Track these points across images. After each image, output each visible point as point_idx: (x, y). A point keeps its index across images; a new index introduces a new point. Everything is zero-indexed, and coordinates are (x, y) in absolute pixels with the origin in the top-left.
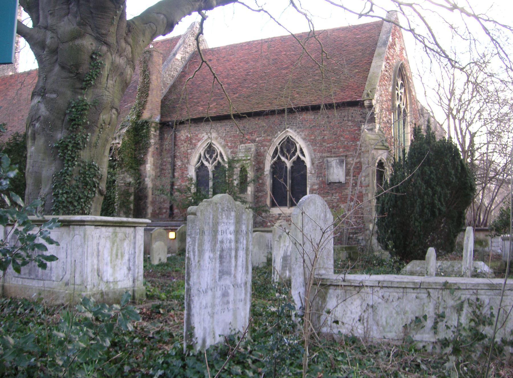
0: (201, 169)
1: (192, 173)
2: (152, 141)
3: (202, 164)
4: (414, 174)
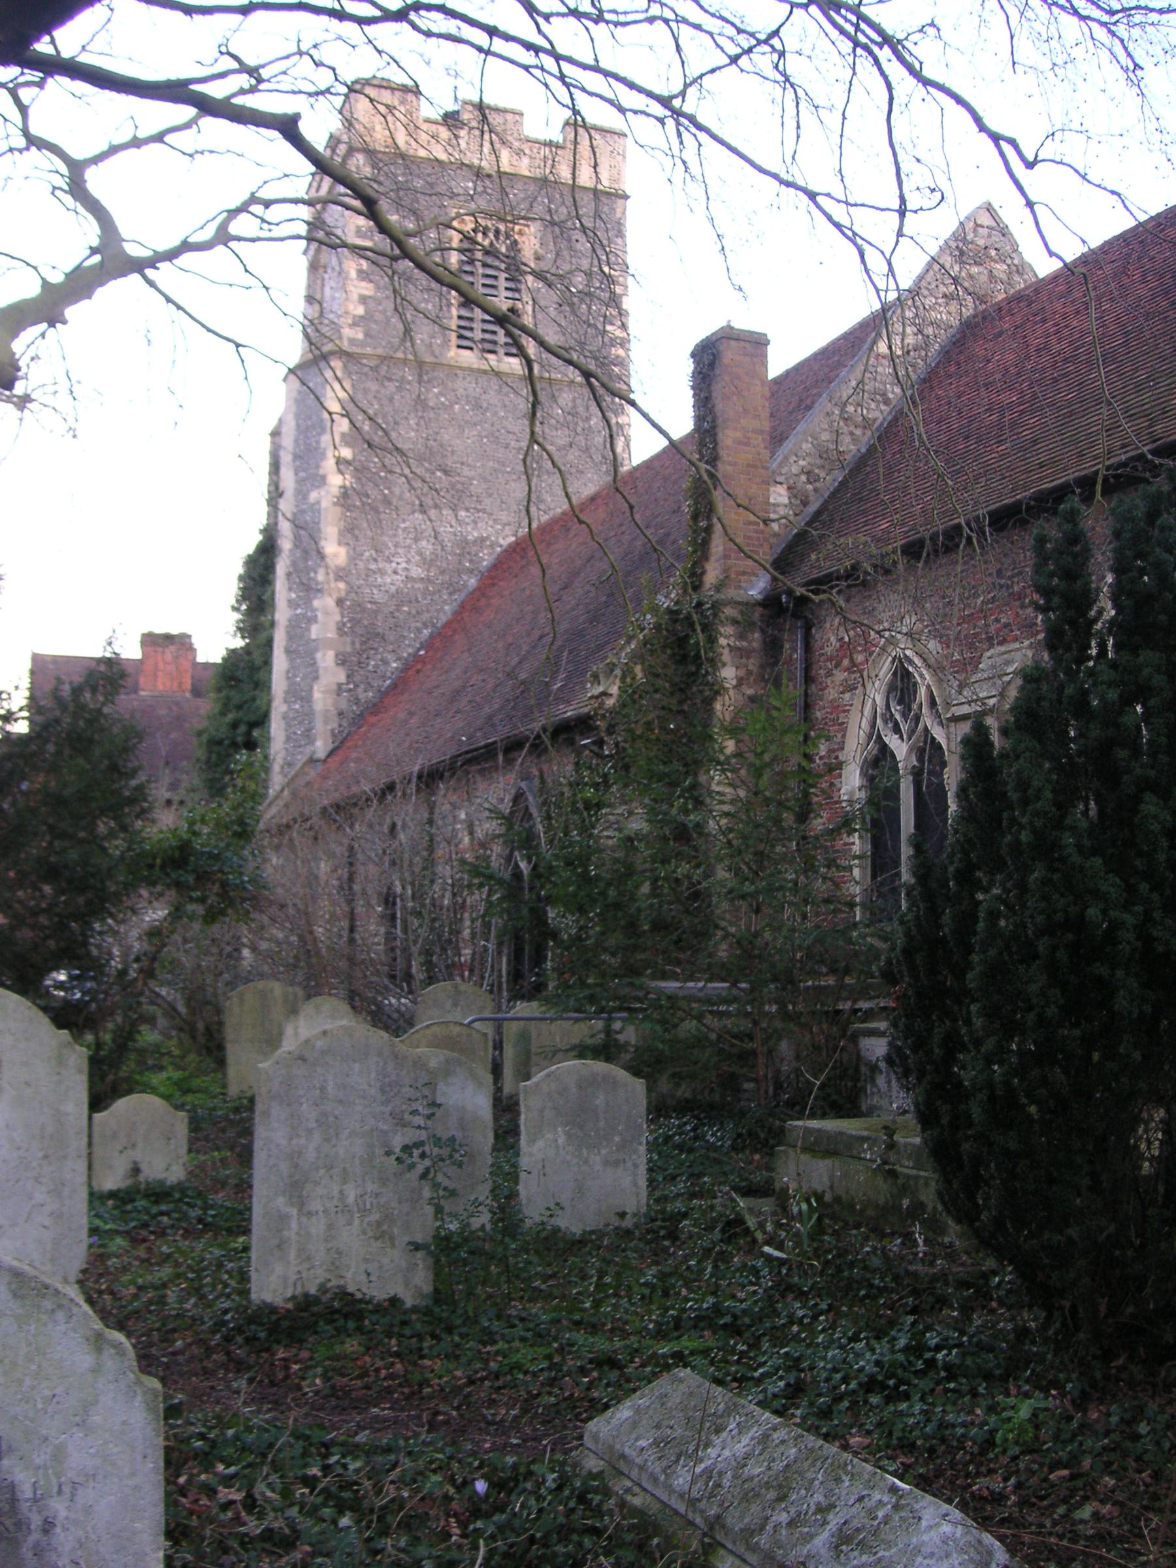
0: (880, 759)
1: (852, 782)
2: (728, 674)
3: (884, 749)
4: (694, 631)
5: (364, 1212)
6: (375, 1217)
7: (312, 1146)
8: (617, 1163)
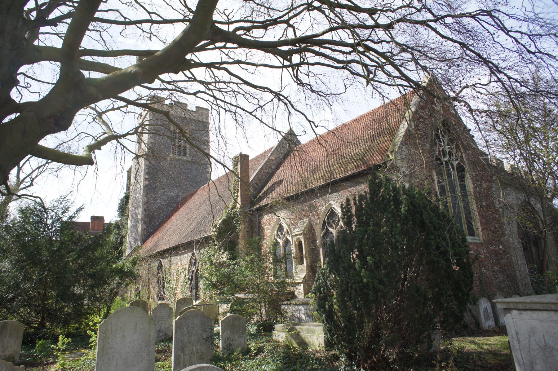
5: (197, 353)
6: (200, 354)
7: (186, 338)
8: (241, 337)
